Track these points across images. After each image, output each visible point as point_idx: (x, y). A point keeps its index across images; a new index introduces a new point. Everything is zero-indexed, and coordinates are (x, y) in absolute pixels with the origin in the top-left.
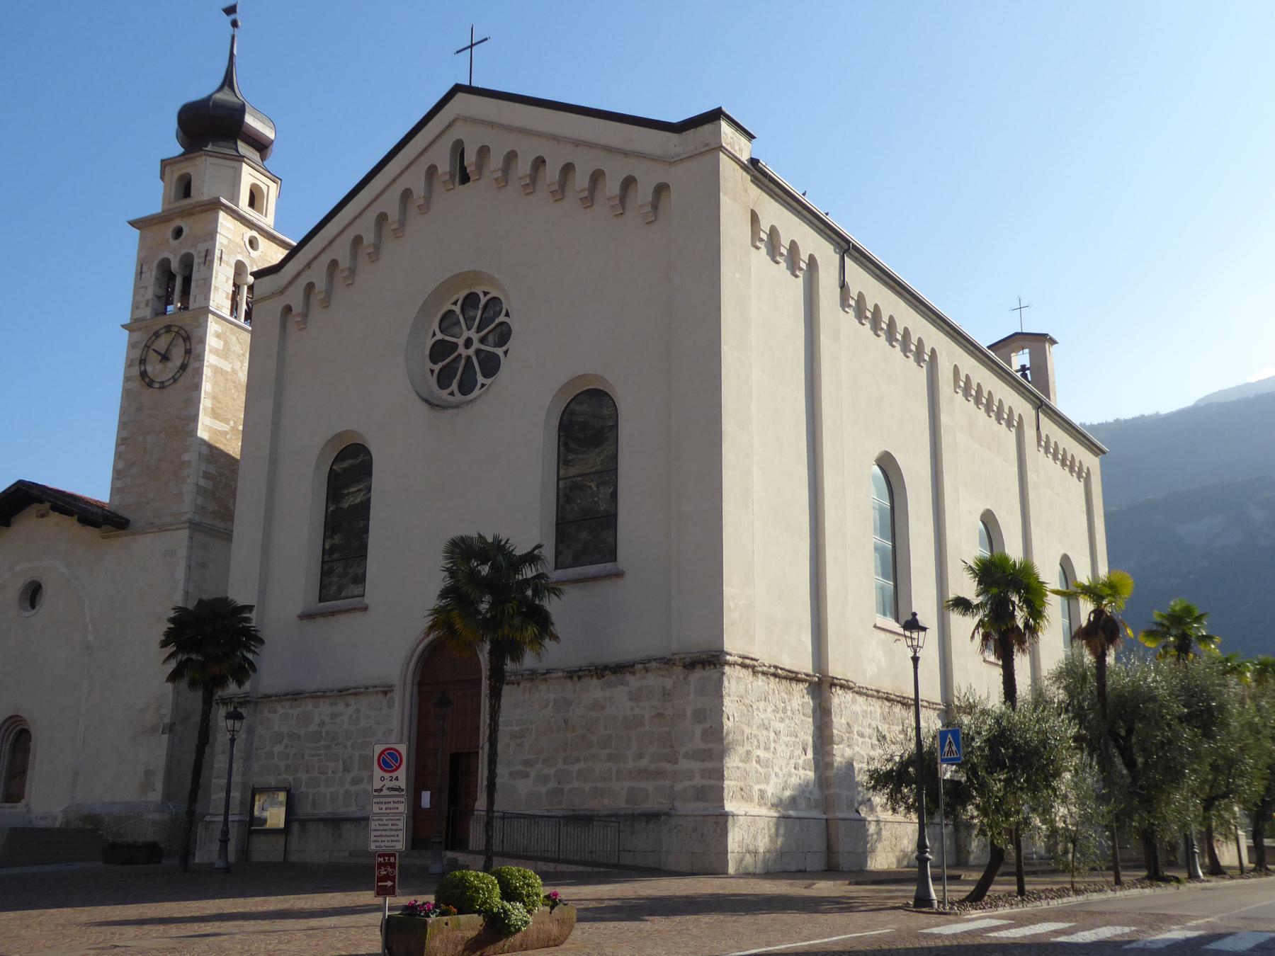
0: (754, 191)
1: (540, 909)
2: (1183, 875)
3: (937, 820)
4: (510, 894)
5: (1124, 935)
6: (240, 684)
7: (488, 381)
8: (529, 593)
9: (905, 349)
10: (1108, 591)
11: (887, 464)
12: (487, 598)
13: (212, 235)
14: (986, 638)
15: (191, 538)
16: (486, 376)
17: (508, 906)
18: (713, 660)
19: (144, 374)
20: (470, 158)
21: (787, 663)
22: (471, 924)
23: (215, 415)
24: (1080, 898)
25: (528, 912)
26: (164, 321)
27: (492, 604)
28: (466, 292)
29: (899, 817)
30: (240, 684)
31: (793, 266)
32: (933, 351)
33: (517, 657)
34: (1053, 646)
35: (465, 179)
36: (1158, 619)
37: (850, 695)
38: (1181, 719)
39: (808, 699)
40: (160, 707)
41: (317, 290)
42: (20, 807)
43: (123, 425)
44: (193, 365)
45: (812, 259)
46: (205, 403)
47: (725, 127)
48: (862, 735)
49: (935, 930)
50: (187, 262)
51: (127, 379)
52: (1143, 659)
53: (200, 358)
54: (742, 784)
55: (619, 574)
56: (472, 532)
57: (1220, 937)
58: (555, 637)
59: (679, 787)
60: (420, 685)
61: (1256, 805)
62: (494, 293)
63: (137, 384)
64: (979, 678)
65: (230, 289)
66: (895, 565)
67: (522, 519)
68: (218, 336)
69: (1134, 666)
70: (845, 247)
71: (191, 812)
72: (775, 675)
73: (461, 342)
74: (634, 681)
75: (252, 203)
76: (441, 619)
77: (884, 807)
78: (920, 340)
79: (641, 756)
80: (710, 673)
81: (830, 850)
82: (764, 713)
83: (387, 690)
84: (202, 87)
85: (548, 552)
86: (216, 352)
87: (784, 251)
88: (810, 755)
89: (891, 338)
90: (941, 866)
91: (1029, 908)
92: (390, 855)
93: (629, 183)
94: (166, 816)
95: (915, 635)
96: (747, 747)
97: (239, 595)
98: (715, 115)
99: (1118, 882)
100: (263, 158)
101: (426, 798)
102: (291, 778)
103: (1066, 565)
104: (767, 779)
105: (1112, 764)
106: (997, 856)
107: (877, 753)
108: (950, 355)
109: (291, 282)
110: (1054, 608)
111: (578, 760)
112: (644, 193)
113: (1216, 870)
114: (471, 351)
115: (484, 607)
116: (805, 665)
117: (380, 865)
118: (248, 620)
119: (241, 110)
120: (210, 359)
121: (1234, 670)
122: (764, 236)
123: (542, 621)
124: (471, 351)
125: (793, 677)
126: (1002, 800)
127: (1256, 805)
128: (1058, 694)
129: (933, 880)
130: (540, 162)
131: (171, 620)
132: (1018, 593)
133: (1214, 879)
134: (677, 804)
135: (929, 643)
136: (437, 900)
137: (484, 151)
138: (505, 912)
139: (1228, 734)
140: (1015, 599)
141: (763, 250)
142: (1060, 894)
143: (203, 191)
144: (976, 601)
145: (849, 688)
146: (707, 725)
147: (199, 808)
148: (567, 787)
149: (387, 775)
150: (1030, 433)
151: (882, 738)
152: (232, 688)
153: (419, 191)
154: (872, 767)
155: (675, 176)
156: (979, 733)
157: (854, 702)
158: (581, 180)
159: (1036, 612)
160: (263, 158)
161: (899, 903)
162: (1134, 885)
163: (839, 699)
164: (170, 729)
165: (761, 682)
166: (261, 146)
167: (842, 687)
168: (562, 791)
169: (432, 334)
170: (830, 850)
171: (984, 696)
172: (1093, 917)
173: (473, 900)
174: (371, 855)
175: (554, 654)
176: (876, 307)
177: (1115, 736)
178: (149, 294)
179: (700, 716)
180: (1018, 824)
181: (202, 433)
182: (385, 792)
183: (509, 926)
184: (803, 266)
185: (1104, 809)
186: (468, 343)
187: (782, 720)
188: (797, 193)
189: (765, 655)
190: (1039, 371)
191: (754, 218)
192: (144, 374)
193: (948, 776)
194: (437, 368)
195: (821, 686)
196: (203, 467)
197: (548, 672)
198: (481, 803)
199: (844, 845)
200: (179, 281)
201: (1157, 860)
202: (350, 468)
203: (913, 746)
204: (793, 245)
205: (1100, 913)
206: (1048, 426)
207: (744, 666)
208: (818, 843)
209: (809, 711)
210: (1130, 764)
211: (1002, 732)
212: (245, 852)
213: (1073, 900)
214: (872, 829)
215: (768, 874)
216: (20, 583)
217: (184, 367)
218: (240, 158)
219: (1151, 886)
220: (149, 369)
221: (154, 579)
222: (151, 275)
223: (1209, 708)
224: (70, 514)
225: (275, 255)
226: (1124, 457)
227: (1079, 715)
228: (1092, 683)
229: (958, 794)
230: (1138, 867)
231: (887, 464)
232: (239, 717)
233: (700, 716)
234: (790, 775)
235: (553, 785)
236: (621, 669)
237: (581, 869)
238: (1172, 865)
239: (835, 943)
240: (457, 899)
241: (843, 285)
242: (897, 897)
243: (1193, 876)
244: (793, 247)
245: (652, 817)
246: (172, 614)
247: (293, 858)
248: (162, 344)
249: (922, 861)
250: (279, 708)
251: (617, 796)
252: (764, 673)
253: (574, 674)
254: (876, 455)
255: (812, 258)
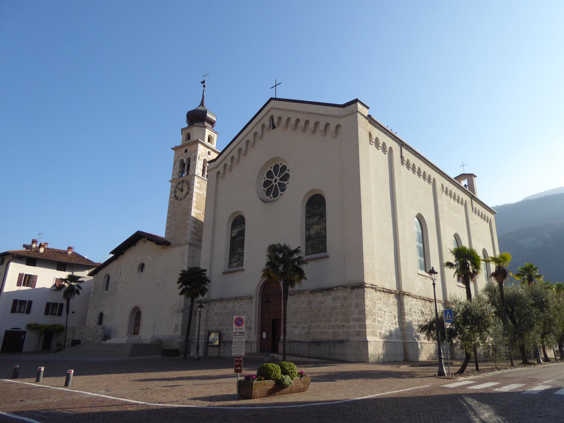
0: (370, 126)
1: (296, 378)
2: (535, 362)
3: (445, 343)
4: (285, 372)
5: (520, 388)
6: (203, 296)
7: (282, 193)
8: (296, 263)
9: (424, 178)
10: (502, 260)
11: (420, 218)
12: (282, 265)
13: (196, 151)
14: (459, 276)
15: (189, 248)
16: (281, 191)
17: (284, 377)
18: (361, 286)
19: (175, 196)
20: (276, 121)
21: (387, 287)
22: (270, 384)
23: (197, 208)
24: (500, 372)
25: (292, 379)
26: (182, 179)
27: (284, 267)
28: (275, 164)
29: (430, 342)
30: (203, 296)
31: (384, 150)
32: (434, 179)
33: (293, 286)
34: (481, 281)
35: (274, 127)
36: (520, 270)
37: (410, 298)
38: (532, 305)
39: (395, 299)
40: (180, 304)
41: (228, 165)
42: (138, 336)
43: (169, 212)
44: (190, 192)
45: (391, 148)
46: (194, 204)
47: (359, 104)
48: (415, 312)
49: (447, 386)
50: (189, 160)
51: (170, 198)
52: (516, 284)
53: (192, 190)
54: (372, 330)
55: (327, 257)
56: (276, 243)
57: (559, 389)
58: (305, 279)
59: (350, 331)
60: (262, 296)
61: (560, 336)
62: (284, 164)
63: (173, 199)
64: (456, 291)
65: (202, 168)
66: (424, 252)
67: (293, 237)
68: (198, 183)
69: (514, 286)
70: (402, 144)
71: (187, 339)
72: (383, 291)
73: (273, 180)
74: (333, 294)
75: (209, 141)
76: (266, 273)
77: (425, 338)
78: (429, 175)
79: (337, 320)
80: (360, 290)
81: (406, 353)
82: (380, 304)
83: (251, 298)
84: (194, 105)
85: (303, 249)
86: (197, 188)
87: (381, 146)
88: (397, 319)
89: (419, 175)
90: (447, 359)
91: (481, 376)
92: (240, 357)
93: (327, 125)
94: (182, 340)
95: (433, 275)
96: (374, 317)
97: (202, 267)
98: (356, 101)
99: (512, 365)
100: (213, 127)
101: (264, 334)
102: (220, 328)
103: (484, 252)
104: (382, 328)
105: (507, 322)
106: (468, 357)
107: (421, 318)
108: (440, 181)
109: (220, 164)
110: (482, 265)
111: (315, 322)
112: (332, 128)
113: (547, 360)
114: (277, 183)
115: (280, 268)
116: (394, 288)
117: (236, 361)
118: (205, 274)
119: (206, 112)
120: (195, 190)
121: (549, 288)
122: (374, 141)
123: (301, 274)
124: (277, 183)
125: (390, 292)
126: (469, 336)
127: (560, 336)
128: (486, 297)
129: (445, 364)
130: (298, 120)
131: (180, 275)
132: (470, 260)
133: (547, 363)
134: (350, 337)
135: (438, 277)
136: (258, 374)
137: (280, 118)
138: (283, 379)
139: (550, 310)
140: (469, 262)
141: (374, 145)
142: (492, 370)
143: (194, 138)
144: (455, 263)
145: (410, 296)
146: (359, 309)
147: (190, 338)
148: (311, 331)
149: (238, 327)
150: (469, 207)
151: (423, 313)
152: (200, 297)
153: (259, 132)
154: (420, 323)
155: (342, 122)
156: (459, 311)
157: (412, 300)
158: (311, 125)
159: (477, 267)
160: (213, 127)
161: (432, 374)
162: (518, 366)
163: (406, 299)
164: (183, 311)
165: (378, 293)
166: (212, 123)
167: (407, 295)
168: (309, 332)
169: (264, 178)
170: (406, 353)
171: (460, 297)
172: (506, 380)
173: (270, 375)
174: (233, 357)
175: (305, 285)
176: (414, 164)
177: (508, 312)
178: (177, 171)
179: (357, 306)
180: (475, 344)
181: (193, 214)
182: (238, 334)
183: (284, 385)
184: (388, 150)
185: (506, 338)
186: (276, 181)
187: (386, 307)
188: (385, 126)
189: (379, 284)
190: (471, 186)
191: (370, 134)
192: (175, 196)
193: (448, 327)
194: (266, 189)
195: (400, 295)
196: (193, 225)
197: (304, 291)
198: (282, 337)
199: (410, 352)
200: (186, 166)
201: (526, 356)
202: (238, 222)
203: (434, 315)
204: (384, 144)
205: (509, 378)
206: (475, 204)
207: (372, 288)
208: (400, 350)
209: (396, 304)
210: (514, 322)
211: (468, 310)
212: (206, 353)
213: (497, 372)
214: (419, 346)
215: (384, 363)
216: (138, 263)
217: (187, 193)
218: (205, 127)
219: (525, 366)
220: (177, 194)
221: (178, 261)
222: (178, 164)
223: (542, 301)
224: (153, 241)
225: (214, 156)
226: (503, 216)
227: (494, 304)
228: (498, 293)
229: (452, 333)
230: (517, 359)
231: (420, 218)
232: (202, 307)
233: (357, 306)
234: (390, 326)
235: (307, 330)
236: (329, 290)
237: (317, 360)
238: (530, 358)
239: (409, 391)
240: (265, 374)
241: (402, 157)
242: (431, 372)
243: (539, 362)
244: (384, 144)
245: (341, 342)
246: (181, 272)
247: (222, 355)
248: (180, 187)
249: (440, 359)
250: (216, 303)
251: (329, 334)
252: (379, 291)
253: (313, 292)
254: (416, 214)
255: (390, 148)
